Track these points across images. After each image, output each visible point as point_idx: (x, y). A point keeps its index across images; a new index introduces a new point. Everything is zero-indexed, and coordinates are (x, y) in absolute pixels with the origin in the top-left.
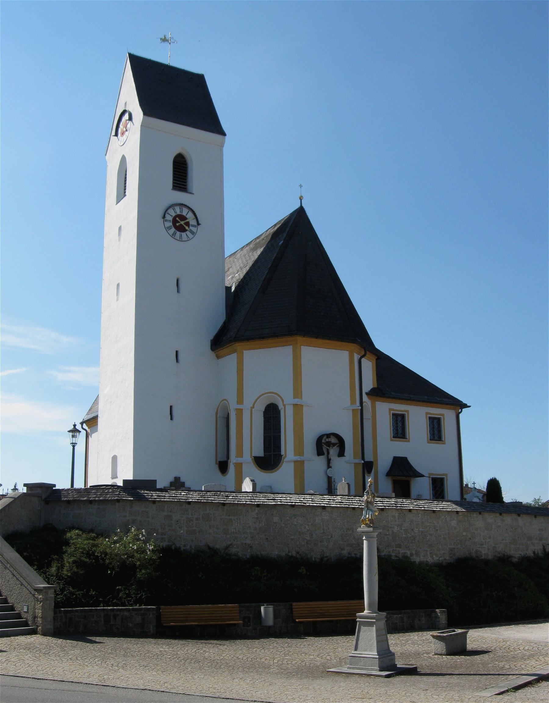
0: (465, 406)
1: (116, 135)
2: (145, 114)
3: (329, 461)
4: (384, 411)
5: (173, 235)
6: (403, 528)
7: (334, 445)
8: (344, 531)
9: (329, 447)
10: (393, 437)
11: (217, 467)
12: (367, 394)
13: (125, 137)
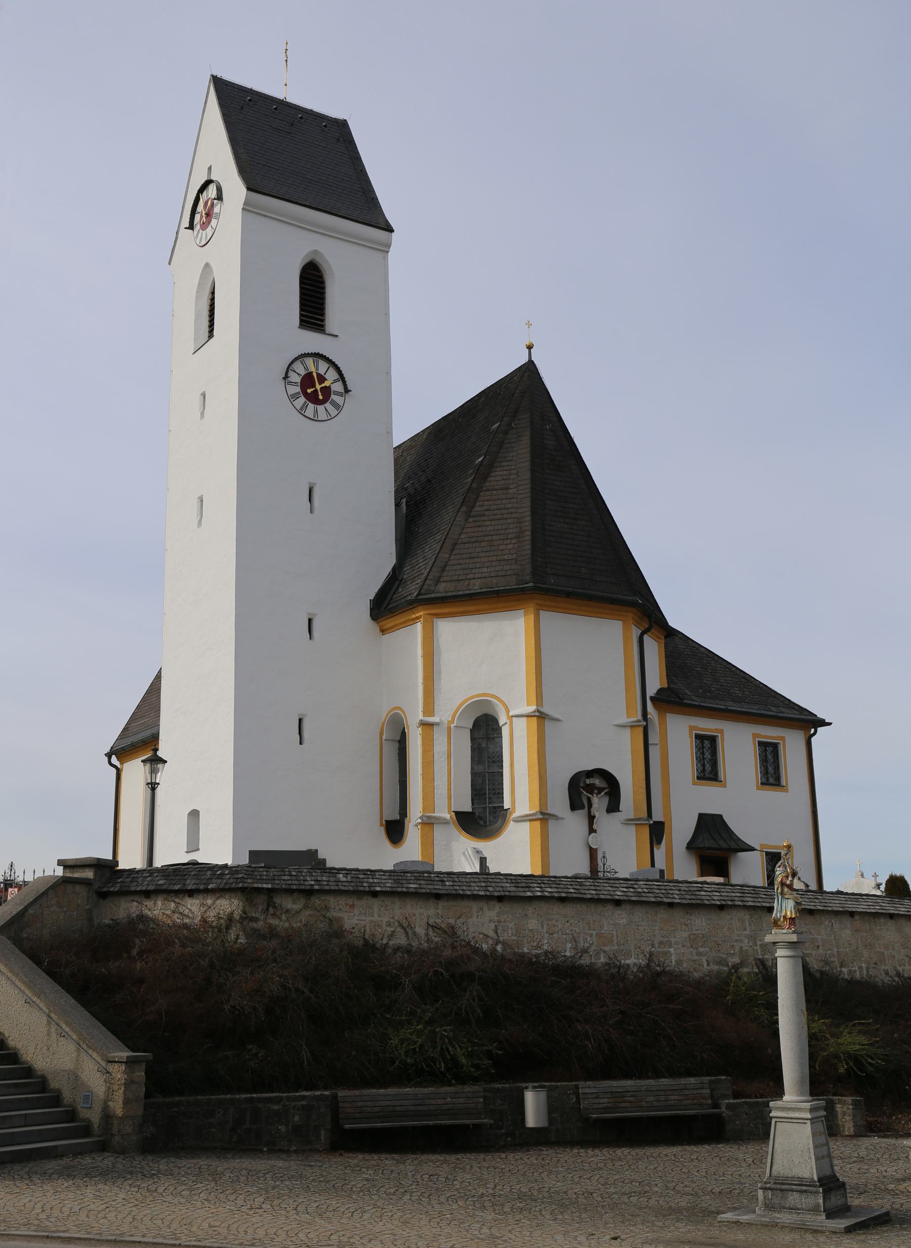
1: (191, 227)
2: (249, 189)
3: (591, 819)
4: (679, 733)
6: (759, 943)
7: (600, 790)
8: (653, 946)
9: (592, 794)
10: (698, 778)
11: (382, 832)
12: (652, 698)
13: (209, 230)
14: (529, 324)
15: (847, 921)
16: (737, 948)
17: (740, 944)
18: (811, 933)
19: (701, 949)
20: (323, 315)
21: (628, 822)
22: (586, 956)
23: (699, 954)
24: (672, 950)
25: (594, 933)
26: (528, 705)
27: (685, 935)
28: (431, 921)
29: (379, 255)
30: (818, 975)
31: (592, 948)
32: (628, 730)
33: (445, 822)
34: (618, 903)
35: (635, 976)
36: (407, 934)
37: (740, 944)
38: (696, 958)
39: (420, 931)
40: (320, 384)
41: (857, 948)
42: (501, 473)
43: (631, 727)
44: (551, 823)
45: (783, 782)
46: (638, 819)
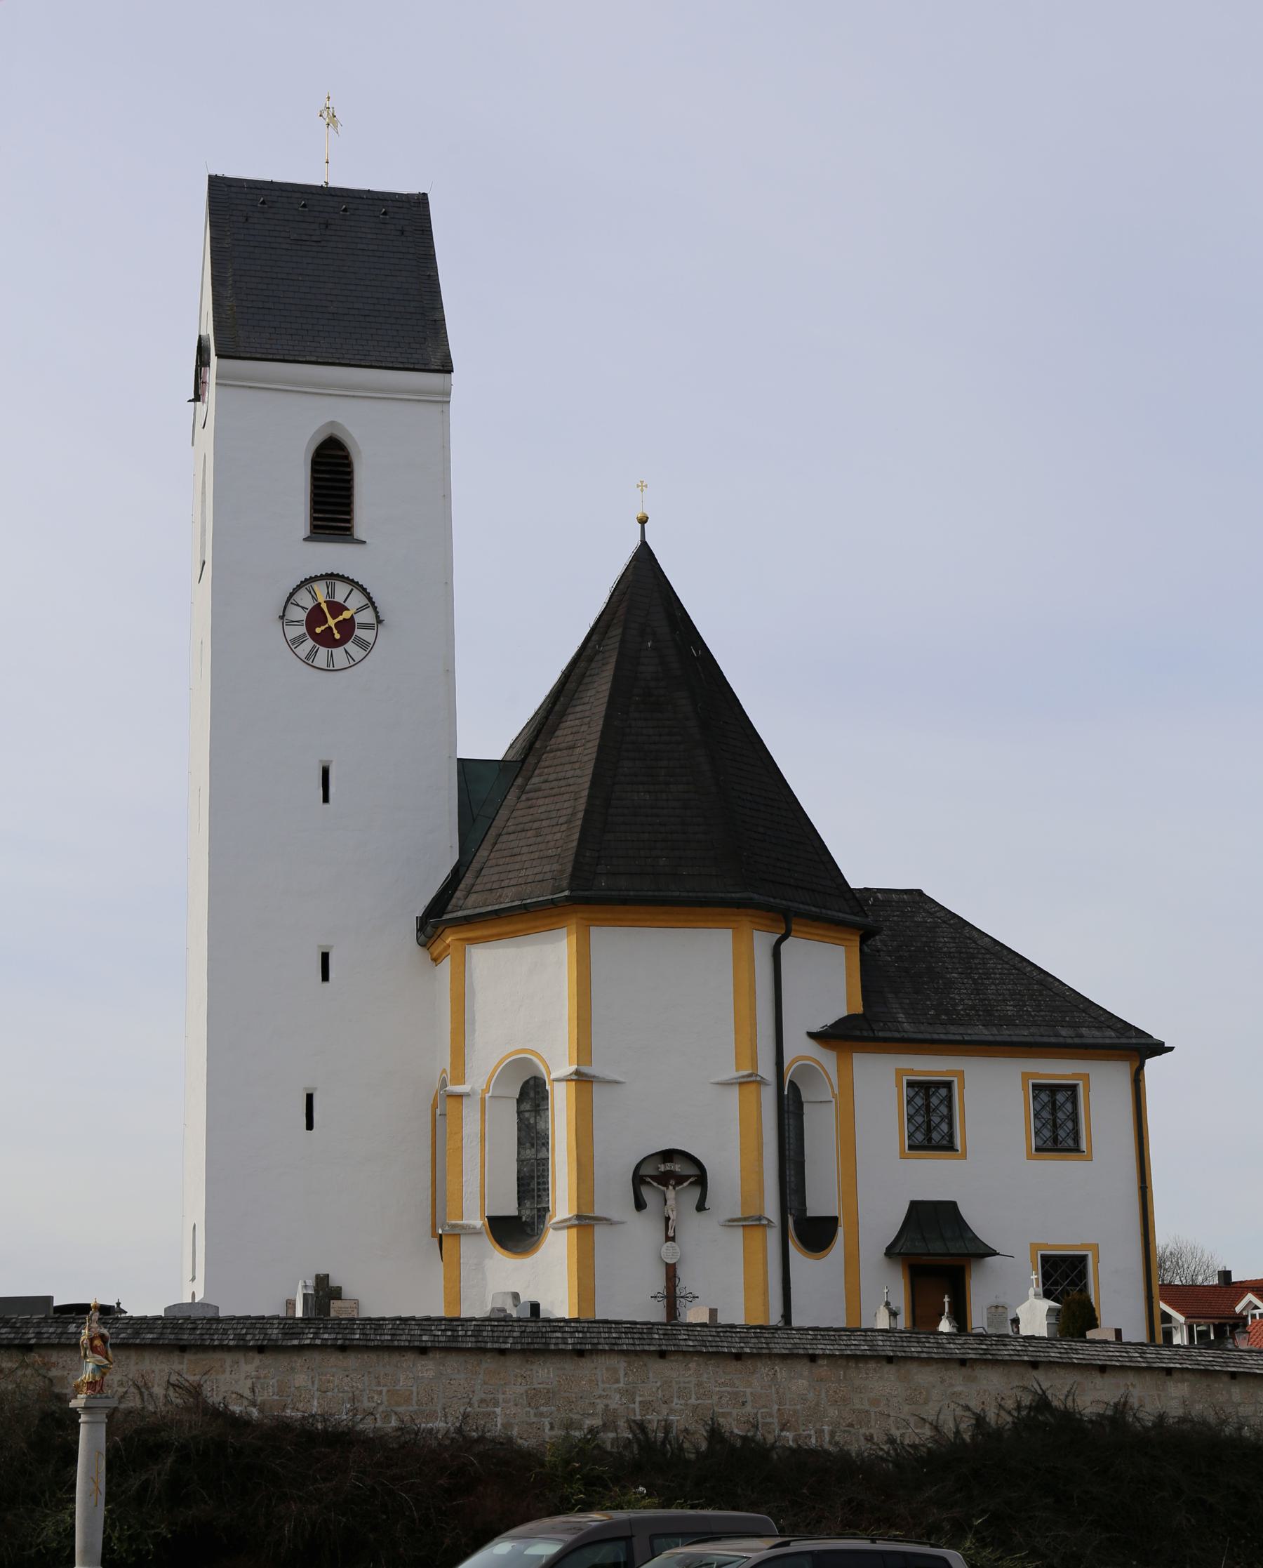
0: (1159, 1049)
5: (308, 657)
6: (638, 1399)
8: (470, 1404)
9: (666, 1185)
14: (642, 486)
15: (803, 1368)
16: (600, 1407)
17: (605, 1401)
18: (733, 1385)
19: (543, 1409)
20: (349, 511)
21: (732, 1222)
22: (369, 1419)
23: (542, 1415)
24: (498, 1410)
25: (385, 1389)
26: (570, 1064)
27: (522, 1389)
28: (174, 1379)
29: (438, 408)
30: (738, 1443)
31: (381, 1409)
32: (736, 1089)
33: (474, 1232)
34: (423, 1351)
35: (439, 1444)
36: (141, 1394)
37: (605, 1401)
38: (534, 1420)
39: (158, 1390)
40: (334, 618)
41: (817, 1404)
42: (572, 723)
43: (741, 1084)
44: (600, 1231)
45: (1084, 1146)
46: (745, 1219)
